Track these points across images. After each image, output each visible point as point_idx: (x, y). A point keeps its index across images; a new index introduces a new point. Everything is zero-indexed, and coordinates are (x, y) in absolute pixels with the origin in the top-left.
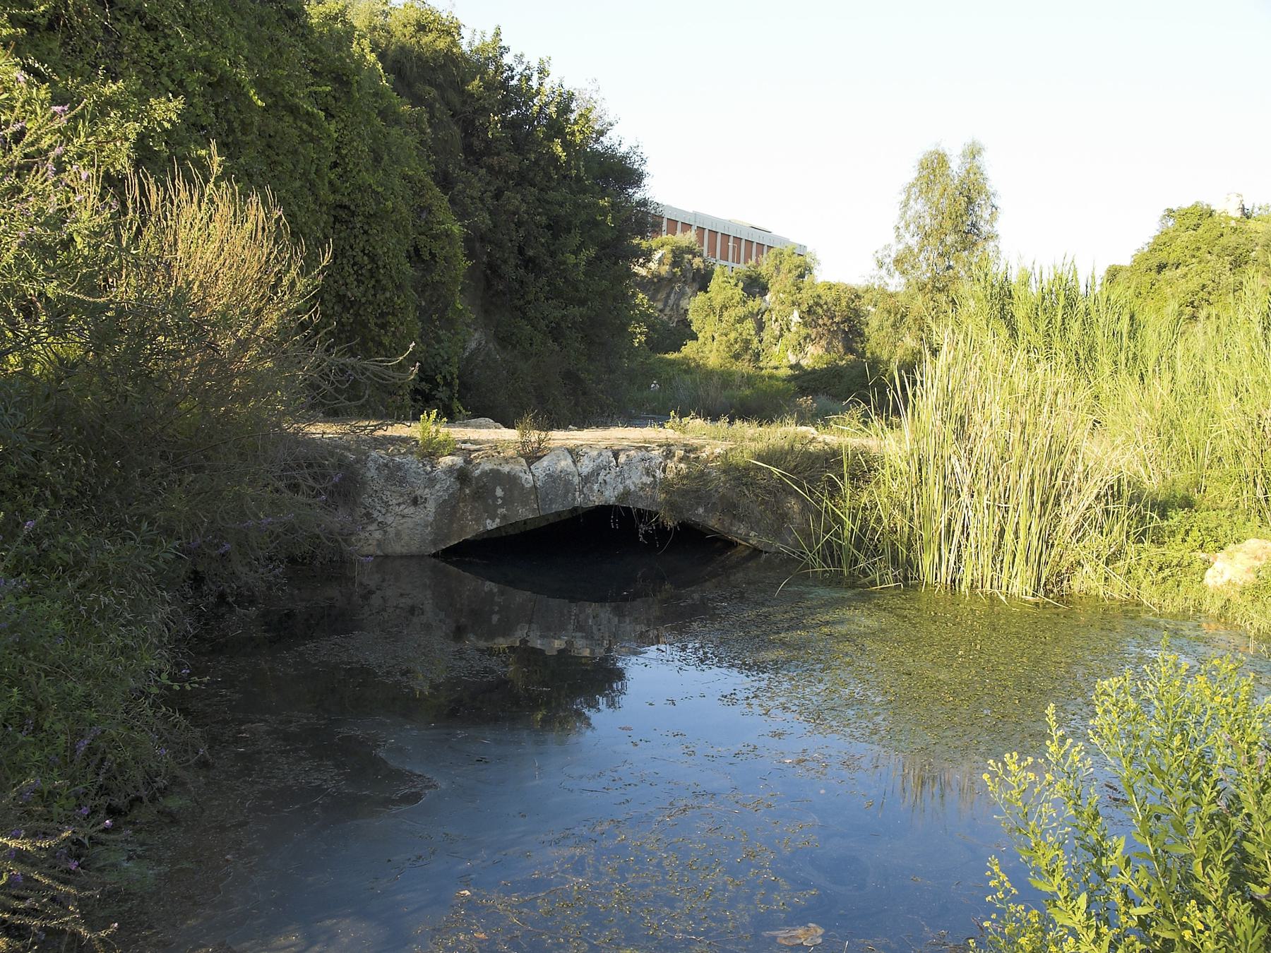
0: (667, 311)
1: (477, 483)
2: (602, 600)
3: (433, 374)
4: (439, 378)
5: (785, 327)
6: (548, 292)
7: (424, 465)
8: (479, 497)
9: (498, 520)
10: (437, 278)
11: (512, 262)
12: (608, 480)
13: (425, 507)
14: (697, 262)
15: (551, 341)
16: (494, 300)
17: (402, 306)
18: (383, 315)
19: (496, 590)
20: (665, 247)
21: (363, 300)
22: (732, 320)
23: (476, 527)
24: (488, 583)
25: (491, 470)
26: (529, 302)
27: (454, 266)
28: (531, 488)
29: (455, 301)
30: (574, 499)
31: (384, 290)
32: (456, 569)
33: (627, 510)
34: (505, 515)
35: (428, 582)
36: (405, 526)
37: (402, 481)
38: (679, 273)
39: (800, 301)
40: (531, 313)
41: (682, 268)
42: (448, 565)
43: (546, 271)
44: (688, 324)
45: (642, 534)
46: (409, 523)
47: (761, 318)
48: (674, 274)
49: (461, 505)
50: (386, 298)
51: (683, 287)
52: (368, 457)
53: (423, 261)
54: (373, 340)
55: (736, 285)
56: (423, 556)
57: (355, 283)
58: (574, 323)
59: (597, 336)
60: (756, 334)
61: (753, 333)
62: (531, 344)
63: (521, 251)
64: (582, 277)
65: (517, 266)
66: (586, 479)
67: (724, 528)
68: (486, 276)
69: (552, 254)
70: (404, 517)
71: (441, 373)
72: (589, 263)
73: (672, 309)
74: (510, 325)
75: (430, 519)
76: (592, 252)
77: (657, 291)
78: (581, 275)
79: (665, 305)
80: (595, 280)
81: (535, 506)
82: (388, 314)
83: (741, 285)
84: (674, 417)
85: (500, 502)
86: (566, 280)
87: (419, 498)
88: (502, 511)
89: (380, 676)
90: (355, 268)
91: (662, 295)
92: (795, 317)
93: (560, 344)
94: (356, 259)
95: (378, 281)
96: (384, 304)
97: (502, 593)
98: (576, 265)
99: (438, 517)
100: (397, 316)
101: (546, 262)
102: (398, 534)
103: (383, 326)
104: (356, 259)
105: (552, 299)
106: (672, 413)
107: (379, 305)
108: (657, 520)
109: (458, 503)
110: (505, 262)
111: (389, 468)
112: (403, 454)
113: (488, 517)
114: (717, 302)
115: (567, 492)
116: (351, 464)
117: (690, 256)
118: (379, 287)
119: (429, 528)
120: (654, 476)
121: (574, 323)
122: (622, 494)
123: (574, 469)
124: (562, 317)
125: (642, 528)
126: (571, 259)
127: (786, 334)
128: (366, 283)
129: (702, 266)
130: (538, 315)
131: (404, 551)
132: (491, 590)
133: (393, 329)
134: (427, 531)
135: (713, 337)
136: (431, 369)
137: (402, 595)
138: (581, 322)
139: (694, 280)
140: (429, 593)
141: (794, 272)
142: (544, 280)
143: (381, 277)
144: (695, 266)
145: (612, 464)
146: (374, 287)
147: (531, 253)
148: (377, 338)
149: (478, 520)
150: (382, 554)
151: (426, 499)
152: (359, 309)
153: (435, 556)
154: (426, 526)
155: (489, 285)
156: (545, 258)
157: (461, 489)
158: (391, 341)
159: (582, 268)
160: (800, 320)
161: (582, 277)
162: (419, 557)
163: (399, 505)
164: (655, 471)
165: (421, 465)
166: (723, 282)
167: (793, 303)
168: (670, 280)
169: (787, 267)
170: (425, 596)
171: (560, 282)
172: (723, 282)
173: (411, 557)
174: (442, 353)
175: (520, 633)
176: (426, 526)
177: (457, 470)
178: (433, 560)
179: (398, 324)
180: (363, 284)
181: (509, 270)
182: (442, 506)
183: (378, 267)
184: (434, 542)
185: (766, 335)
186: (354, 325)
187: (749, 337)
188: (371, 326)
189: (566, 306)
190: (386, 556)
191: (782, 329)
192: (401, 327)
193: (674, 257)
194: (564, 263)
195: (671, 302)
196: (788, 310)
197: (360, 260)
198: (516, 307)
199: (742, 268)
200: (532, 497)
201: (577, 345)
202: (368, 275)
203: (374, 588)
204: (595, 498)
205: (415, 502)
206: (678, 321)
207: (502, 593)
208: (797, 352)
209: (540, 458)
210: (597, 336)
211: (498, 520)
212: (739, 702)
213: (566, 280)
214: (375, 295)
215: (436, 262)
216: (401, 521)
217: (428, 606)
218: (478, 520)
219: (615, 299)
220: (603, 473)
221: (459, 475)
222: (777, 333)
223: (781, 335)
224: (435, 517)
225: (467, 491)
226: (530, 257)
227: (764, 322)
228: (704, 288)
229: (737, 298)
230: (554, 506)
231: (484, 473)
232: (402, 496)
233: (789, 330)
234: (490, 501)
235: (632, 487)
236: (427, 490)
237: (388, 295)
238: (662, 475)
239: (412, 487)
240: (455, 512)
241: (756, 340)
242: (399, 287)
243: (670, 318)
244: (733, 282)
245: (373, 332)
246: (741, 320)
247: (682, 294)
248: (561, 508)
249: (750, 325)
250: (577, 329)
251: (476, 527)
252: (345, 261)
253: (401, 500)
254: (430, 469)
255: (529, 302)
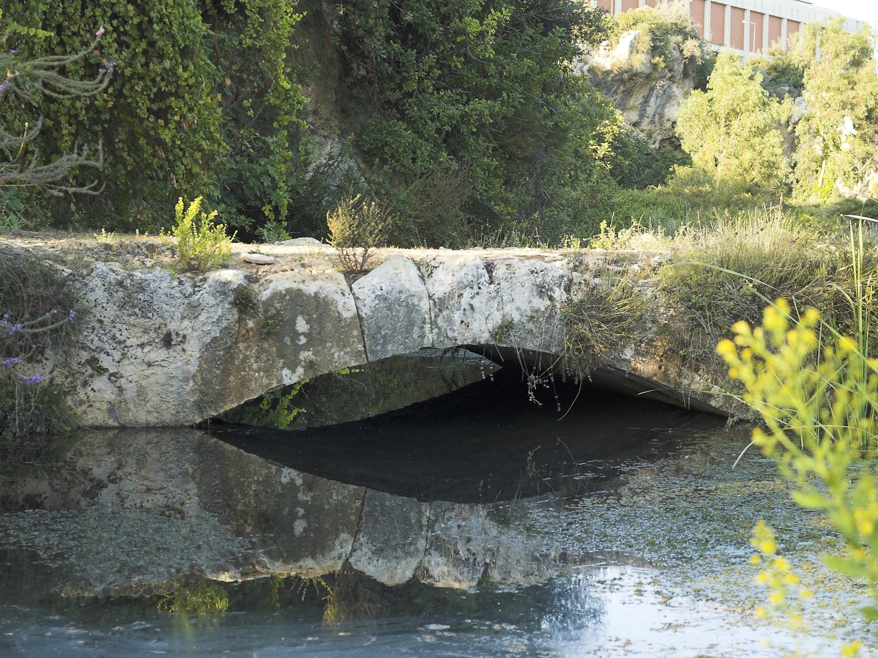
0: (645, 125)
1: (266, 311)
2: (472, 499)
3: (258, 203)
4: (267, 210)
5: (830, 144)
6: (439, 78)
7: (181, 283)
8: (269, 334)
9: (300, 370)
10: (249, 41)
11: (381, 31)
12: (476, 305)
13: (184, 350)
14: (690, 47)
15: (445, 154)
16: (354, 92)
17: (192, 81)
18: (161, 96)
19: (299, 482)
20: (639, 25)
21: (128, 72)
22: (745, 134)
23: (265, 381)
24: (286, 471)
25: (289, 291)
26: (410, 95)
27: (275, 23)
28: (352, 318)
29: (276, 78)
30: (422, 336)
31: (162, 57)
32: (234, 448)
33: (510, 351)
34: (311, 362)
35: (191, 470)
36: (152, 379)
37: (147, 309)
38: (663, 65)
39: (854, 101)
40: (414, 111)
41: (666, 57)
42: (221, 443)
43: (435, 45)
44: (674, 142)
45: (533, 390)
46: (159, 375)
47: (793, 132)
48: (655, 66)
49: (241, 346)
50: (164, 69)
51: (669, 87)
52: (92, 270)
53: (228, 17)
54: (146, 135)
55: (751, 78)
56: (182, 427)
57: (115, 45)
58: (481, 126)
59: (520, 147)
60: (785, 153)
61: (779, 151)
62: (414, 160)
63: (395, 15)
64: (491, 53)
65: (388, 38)
66: (441, 304)
67: (669, 381)
68: (341, 54)
69: (445, 19)
70: (149, 365)
71: (270, 203)
72: (502, 31)
73: (652, 122)
74: (380, 131)
75: (193, 368)
76: (506, 13)
77: (628, 93)
78: (491, 50)
79: (642, 116)
80: (512, 59)
81: (360, 347)
82: (170, 94)
83: (759, 78)
84: (606, 231)
85: (303, 340)
86: (468, 61)
87: (174, 336)
88: (304, 355)
89: (43, 560)
90: (115, 22)
91: (636, 100)
92: (847, 127)
93: (460, 159)
94: (116, 9)
95: (152, 44)
96: (163, 79)
97: (309, 487)
98: (481, 35)
99: (205, 366)
100: (183, 98)
101: (434, 30)
102: (141, 392)
103: (162, 114)
104: (116, 9)
105: (445, 88)
106: (603, 225)
107: (153, 80)
108: (556, 367)
109: (236, 343)
110: (370, 32)
111: (125, 288)
112: (149, 268)
113: (285, 365)
114: (721, 108)
115: (411, 324)
116: (63, 283)
117: (680, 38)
118: (153, 52)
119: (191, 383)
120: (551, 298)
121: (481, 126)
122: (501, 327)
123: (422, 287)
124: (462, 117)
125: (533, 381)
126: (474, 26)
127: (833, 154)
128: (133, 45)
129: (698, 53)
130: (424, 114)
131: (152, 419)
132: (292, 481)
133: (177, 118)
134: (188, 388)
135: (716, 160)
136: (256, 195)
137: (149, 490)
138: (493, 125)
139: (685, 75)
140: (192, 488)
141: (843, 57)
142: (431, 58)
143: (156, 37)
144: (687, 54)
145: (482, 280)
146: (145, 52)
147: (409, 17)
148: (152, 133)
149: (268, 371)
150: (116, 424)
151: (184, 337)
152: (123, 86)
153: (199, 427)
154: (186, 380)
155: (347, 71)
156: (434, 25)
157: (240, 320)
158: (174, 136)
159: (490, 39)
160: (855, 132)
161: (491, 53)
162: (175, 429)
163: (142, 346)
164: (552, 290)
165: (176, 283)
166: (731, 74)
167: (844, 106)
168: (648, 77)
169: (832, 49)
170: (186, 491)
171: (457, 63)
172: (731, 74)
173: (162, 428)
174: (271, 170)
175: (343, 545)
176: (186, 380)
177: (235, 290)
178: (199, 434)
179: (185, 110)
180: (128, 47)
181: (376, 46)
182: (210, 346)
183: (151, 22)
184: (199, 406)
185: (801, 156)
186: (115, 112)
187: (772, 159)
188: (143, 113)
189: (468, 100)
190: (123, 428)
191: (826, 147)
192: (189, 115)
193: (653, 40)
194: (464, 32)
195: (650, 110)
196: (836, 116)
197: (122, 10)
198: (388, 102)
199: (766, 59)
200: (355, 333)
201: (486, 160)
202: (135, 33)
203: (104, 478)
204: (456, 334)
205: (167, 341)
206: (663, 141)
207: (309, 487)
208: (851, 181)
209: (366, 272)
210: (520, 147)
211: (300, 370)
212: (624, 589)
213: (468, 61)
214: (146, 65)
215: (246, 17)
216: (146, 373)
217: (192, 507)
218: (268, 371)
219: (546, 89)
220: (467, 293)
221: (236, 299)
222: (820, 153)
223: (826, 157)
224: (200, 366)
225: (251, 324)
226: (409, 25)
227: (798, 138)
228: (702, 85)
229: (753, 99)
230: (390, 347)
231: (278, 296)
232: (146, 332)
233: (838, 148)
234: (287, 340)
235: (516, 317)
236: (186, 323)
237: (167, 64)
238: (565, 297)
239: (162, 317)
240: (232, 358)
241: (784, 164)
242: (185, 53)
243: (650, 136)
244: (748, 73)
245: (146, 123)
246: (761, 132)
247: (667, 98)
248: (401, 351)
249: (774, 138)
250: (488, 137)
251: (265, 381)
252: (98, 12)
253: (145, 339)
254: (190, 290)
255: (410, 95)
